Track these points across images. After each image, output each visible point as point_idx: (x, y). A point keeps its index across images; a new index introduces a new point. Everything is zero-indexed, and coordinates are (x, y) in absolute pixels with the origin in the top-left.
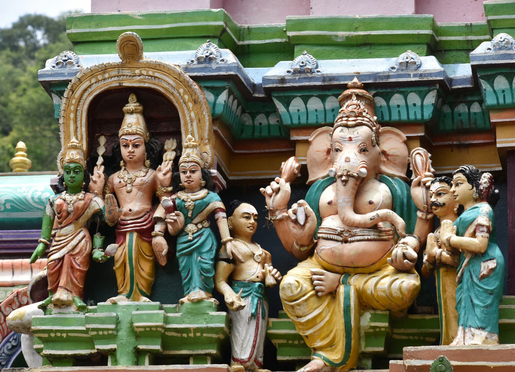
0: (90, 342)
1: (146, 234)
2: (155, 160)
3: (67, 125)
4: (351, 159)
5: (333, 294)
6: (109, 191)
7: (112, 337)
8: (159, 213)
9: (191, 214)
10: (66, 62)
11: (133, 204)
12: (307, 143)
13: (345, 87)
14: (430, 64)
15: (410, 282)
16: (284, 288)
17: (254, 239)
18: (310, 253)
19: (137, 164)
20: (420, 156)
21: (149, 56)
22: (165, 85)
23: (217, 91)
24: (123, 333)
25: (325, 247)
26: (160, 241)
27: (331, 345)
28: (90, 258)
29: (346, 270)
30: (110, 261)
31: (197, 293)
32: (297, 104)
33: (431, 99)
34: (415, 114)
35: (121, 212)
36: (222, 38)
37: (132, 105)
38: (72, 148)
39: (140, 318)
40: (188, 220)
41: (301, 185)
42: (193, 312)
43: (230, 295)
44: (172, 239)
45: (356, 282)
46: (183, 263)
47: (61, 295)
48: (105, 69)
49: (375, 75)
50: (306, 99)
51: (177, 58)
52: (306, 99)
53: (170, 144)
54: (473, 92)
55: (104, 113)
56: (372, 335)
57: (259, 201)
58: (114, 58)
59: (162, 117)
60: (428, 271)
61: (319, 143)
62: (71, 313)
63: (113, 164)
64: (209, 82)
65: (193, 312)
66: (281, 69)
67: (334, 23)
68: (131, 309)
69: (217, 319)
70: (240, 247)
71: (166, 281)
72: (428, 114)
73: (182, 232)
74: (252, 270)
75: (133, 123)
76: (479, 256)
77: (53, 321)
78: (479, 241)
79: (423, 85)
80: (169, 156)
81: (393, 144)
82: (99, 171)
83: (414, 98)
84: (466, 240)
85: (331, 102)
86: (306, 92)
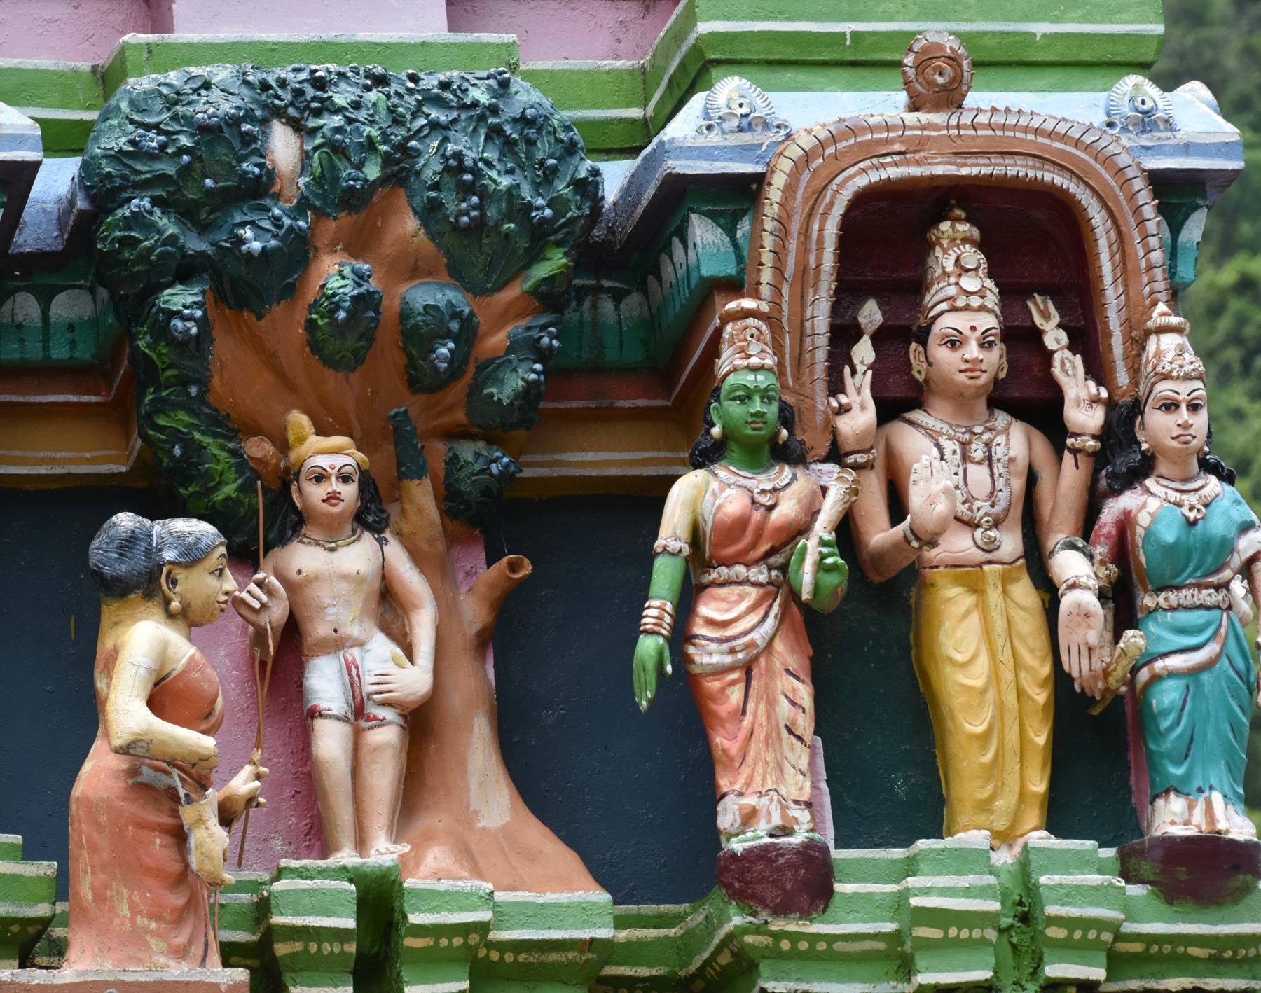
63: (897, 401)
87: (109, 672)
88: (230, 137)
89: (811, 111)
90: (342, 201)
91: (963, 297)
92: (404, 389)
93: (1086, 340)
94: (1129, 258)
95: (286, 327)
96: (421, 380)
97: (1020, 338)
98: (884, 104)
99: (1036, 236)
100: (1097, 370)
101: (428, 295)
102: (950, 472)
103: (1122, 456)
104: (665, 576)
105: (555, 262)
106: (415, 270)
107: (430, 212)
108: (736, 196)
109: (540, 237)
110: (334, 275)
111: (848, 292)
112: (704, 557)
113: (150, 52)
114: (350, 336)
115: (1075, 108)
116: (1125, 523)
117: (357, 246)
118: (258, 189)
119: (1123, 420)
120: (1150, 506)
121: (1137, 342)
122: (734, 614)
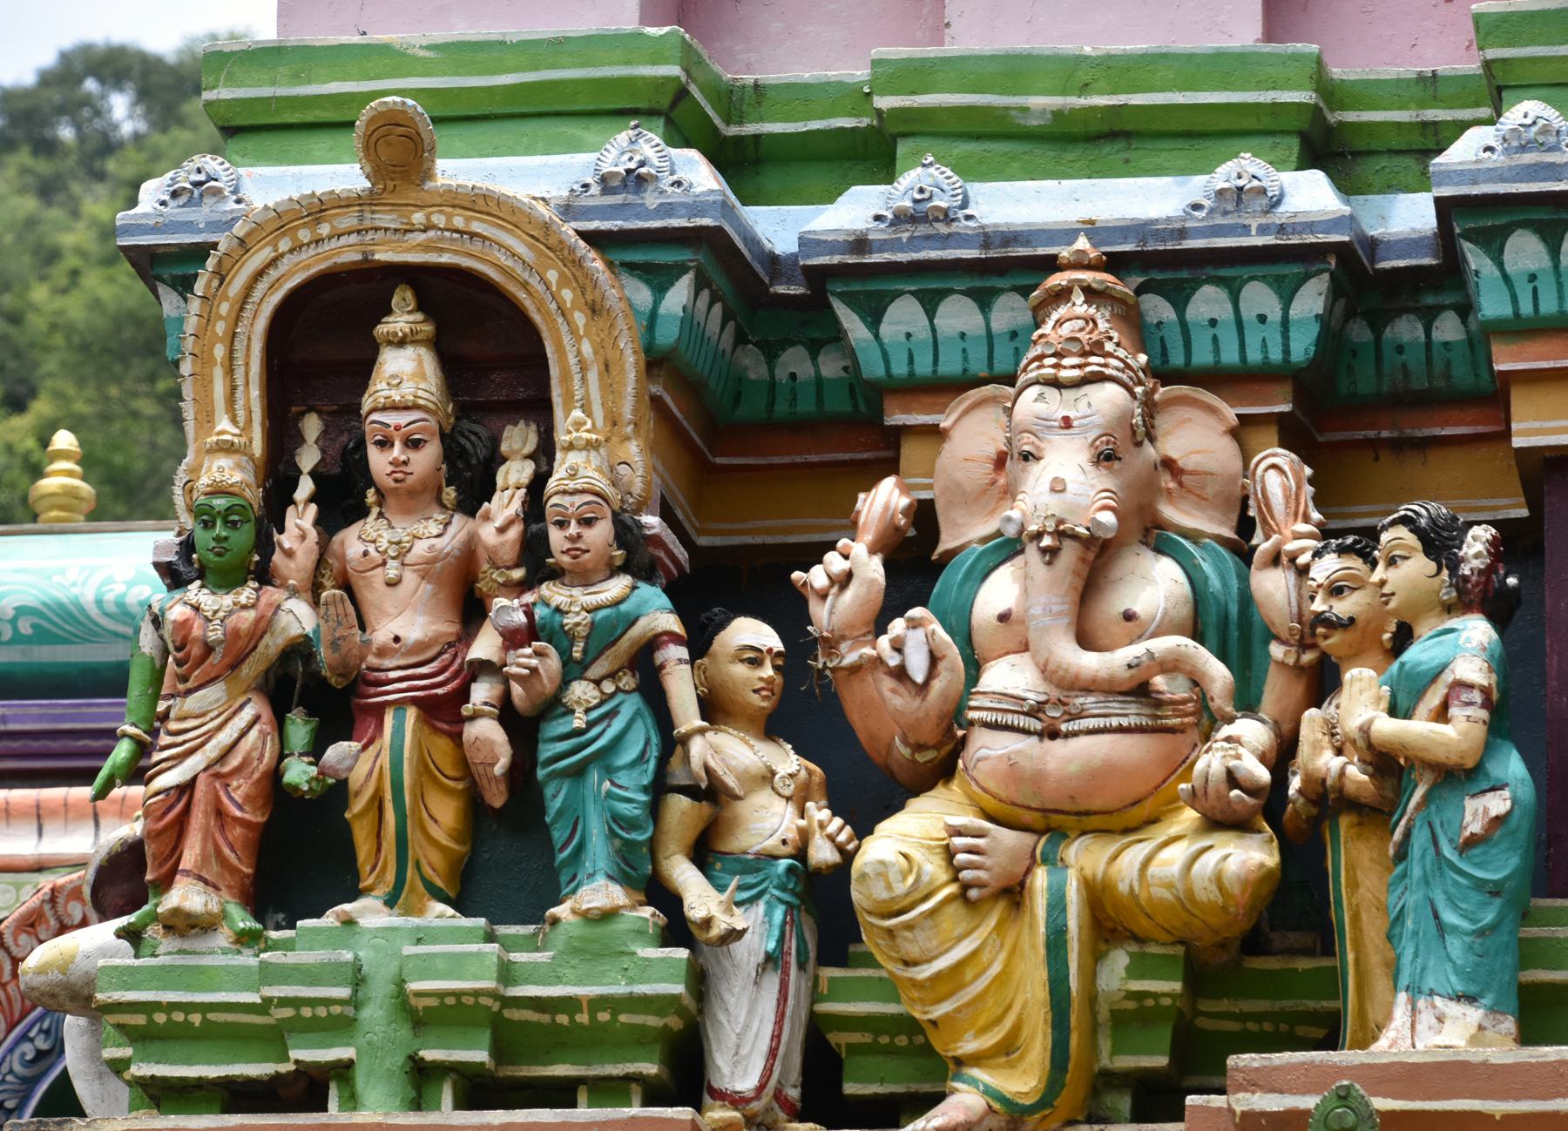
0: (274, 1039)
1: (443, 712)
2: (472, 486)
3: (203, 380)
4: (1068, 482)
5: (1013, 894)
6: (333, 581)
7: (340, 1024)
8: (485, 646)
9: (582, 651)
10: (202, 190)
11: (406, 620)
12: (936, 434)
13: (1051, 264)
14: (1310, 195)
15: (1248, 856)
16: (863, 876)
17: (773, 727)
18: (943, 770)
19: (417, 497)
20: (1280, 475)
21: (455, 170)
22: (501, 257)
23: (659, 278)
24: (375, 1014)
25: (990, 750)
26: (487, 733)
27: (1007, 1050)
28: (274, 785)
29: (1053, 820)
30: (336, 792)
31: (599, 891)
32: (904, 316)
33: (1311, 300)
34: (1263, 347)
35: (368, 643)
36: (677, 115)
37: (402, 319)
38: (220, 451)
39: (427, 967)
40: (573, 670)
41: (915, 562)
42: (589, 949)
43: (700, 897)
44: (522, 726)
45: (1085, 857)
46: (556, 798)
47: (186, 896)
48: (318, 209)
49: (1141, 229)
50: (930, 301)
51: (540, 176)
52: (930, 301)
53: (518, 438)
54: (1439, 278)
55: (317, 345)
56: (1132, 1018)
57: (788, 611)
58: (346, 175)
59: (494, 355)
60: (1302, 823)
61: (972, 434)
62: (218, 951)
63: (344, 497)
64: (637, 250)
65: (589, 949)
66: (855, 210)
67: (1016, 70)
68: (399, 939)
69: (660, 971)
70: (730, 752)
71: (505, 856)
72: (1302, 346)
73: (554, 705)
74: (768, 822)
75: (405, 374)
76: (1458, 777)
77: (163, 977)
78: (1458, 733)
79: (1287, 260)
80: (515, 473)
81: (1197, 436)
82: (301, 520)
83: (1259, 297)
84: (1418, 729)
85: (1009, 311)
86: (931, 281)
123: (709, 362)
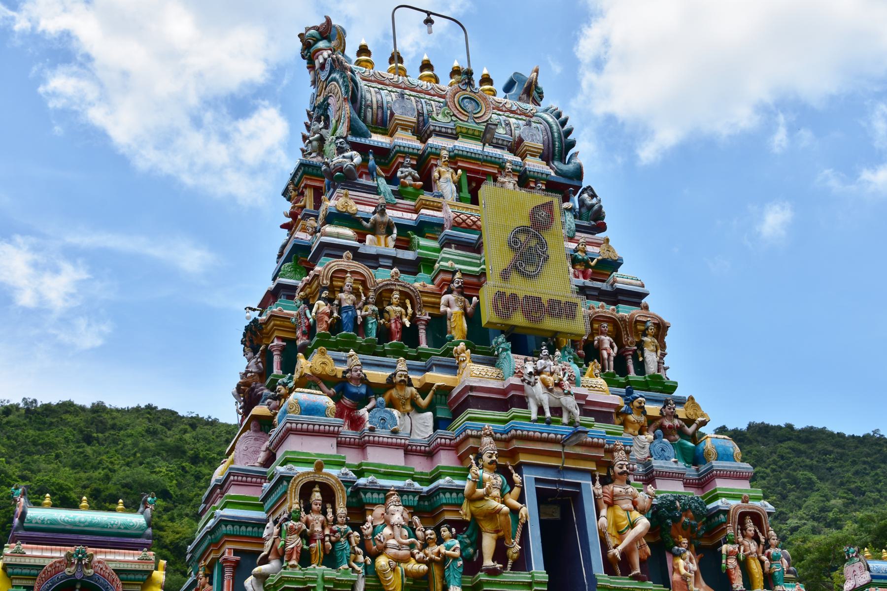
0: (305, 583)
1: (323, 541)
3: (291, 494)
5: (394, 570)
6: (307, 523)
7: (315, 581)
8: (327, 532)
10: (291, 469)
12: (373, 510)
13: (389, 491)
14: (417, 485)
19: (318, 512)
20: (416, 519)
21: (325, 470)
22: (332, 482)
23: (348, 487)
28: (302, 548)
29: (399, 560)
32: (369, 495)
33: (417, 498)
35: (12, 527)
37: (317, 489)
39: (327, 574)
40: (342, 536)
45: (403, 566)
48: (309, 473)
49: (399, 487)
50: (372, 494)
51: (335, 472)
52: (372, 494)
55: (306, 491)
60: (430, 563)
62: (297, 570)
64: (348, 483)
67: (380, 465)
70: (357, 549)
71: (331, 559)
72: (416, 503)
75: (317, 496)
76: (455, 559)
77: (290, 573)
79: (415, 493)
80: (329, 510)
86: (373, 491)
87: (829, 551)
88: (673, 502)
89: (734, 503)
90: (684, 510)
91: (751, 527)
92: (690, 532)
93: (762, 531)
94: (767, 521)
95: (679, 526)
96: (692, 532)
97: (755, 531)
98: (739, 502)
99: (757, 518)
100: (763, 535)
101: (693, 522)
102: (753, 546)
103: (767, 545)
104: (724, 557)
105: (704, 519)
106: (691, 519)
107: (693, 512)
108: (726, 512)
109: (704, 516)
110: (684, 519)
111: (527, 522)
112: (729, 554)
113: (195, 460)
114: (685, 526)
115: (757, 504)
116: (769, 553)
117: (686, 516)
118: (676, 508)
119: (767, 540)
120: (772, 551)
121: (768, 531)
122: (732, 562)
123: (32, 562)
